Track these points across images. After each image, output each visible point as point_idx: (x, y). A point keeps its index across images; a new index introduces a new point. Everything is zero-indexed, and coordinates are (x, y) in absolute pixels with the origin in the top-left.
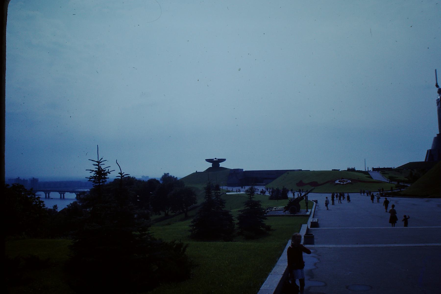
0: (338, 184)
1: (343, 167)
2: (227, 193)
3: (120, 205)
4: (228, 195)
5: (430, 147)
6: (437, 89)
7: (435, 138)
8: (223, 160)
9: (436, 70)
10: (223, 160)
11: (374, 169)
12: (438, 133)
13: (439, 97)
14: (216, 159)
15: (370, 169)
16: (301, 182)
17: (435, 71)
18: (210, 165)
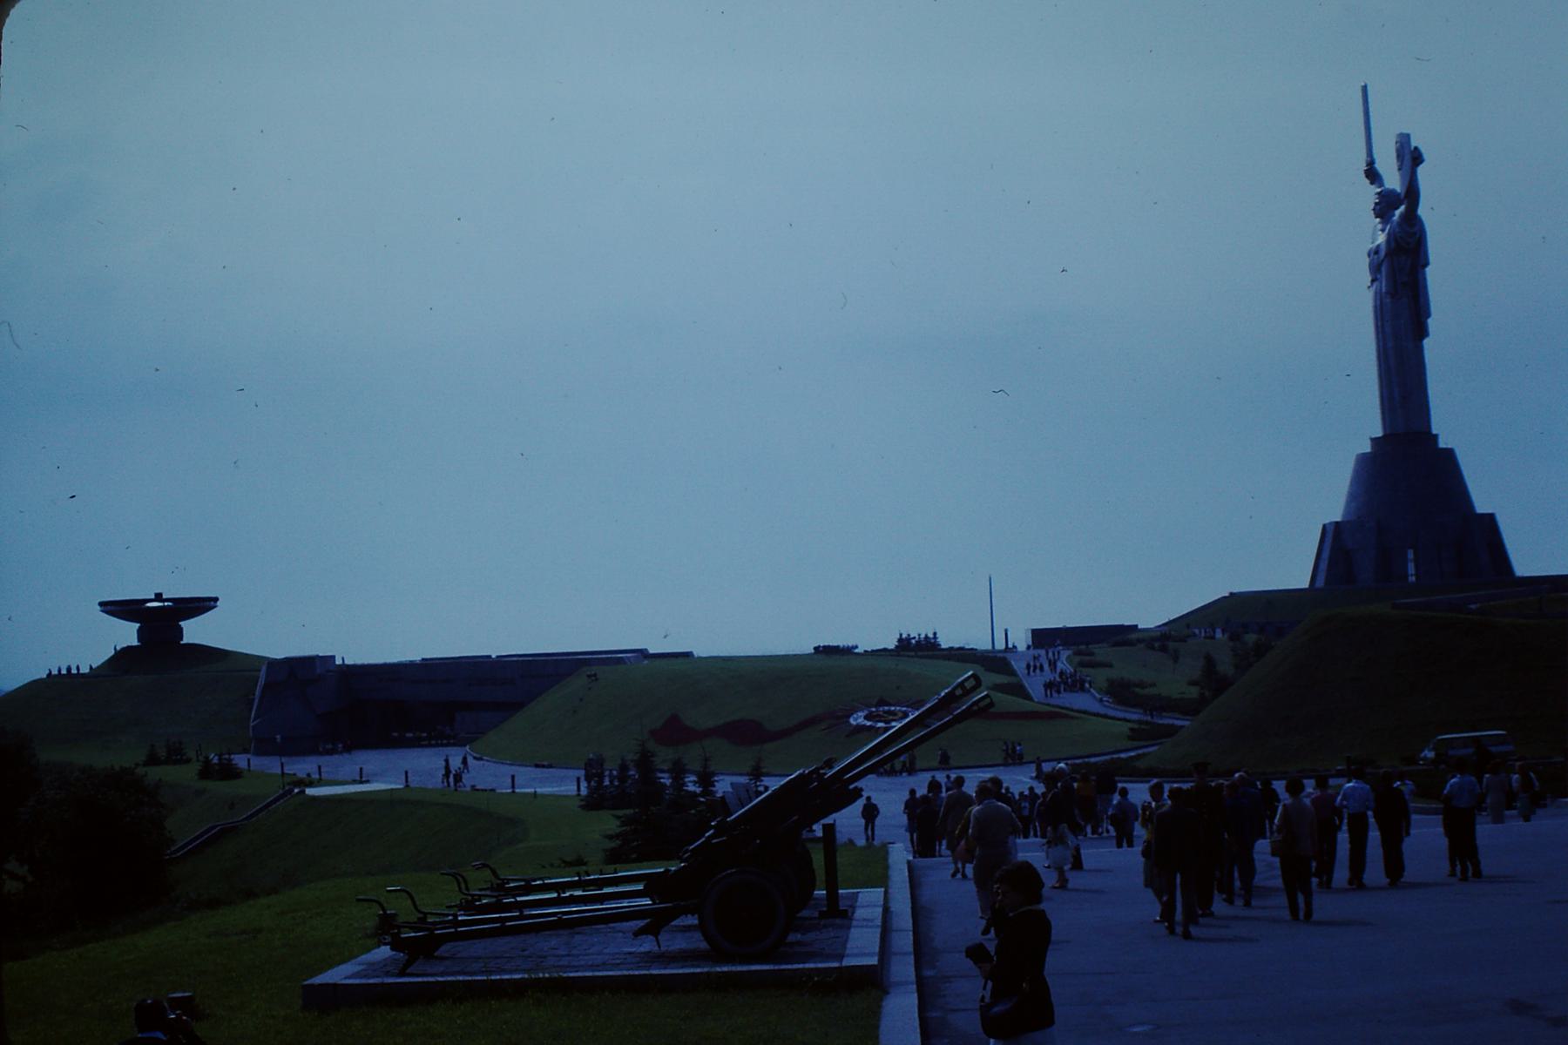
0: (860, 729)
1: (873, 633)
2: (310, 791)
3: (1483, 515)
4: (314, 798)
5: (1335, 511)
6: (1370, 193)
7: (1363, 459)
8: (199, 606)
9: (1365, 89)
10: (199, 606)
11: (1042, 638)
12: (1380, 434)
13: (1381, 238)
14: (158, 597)
15: (1021, 640)
16: (674, 720)
17: (1360, 94)
18: (127, 634)
